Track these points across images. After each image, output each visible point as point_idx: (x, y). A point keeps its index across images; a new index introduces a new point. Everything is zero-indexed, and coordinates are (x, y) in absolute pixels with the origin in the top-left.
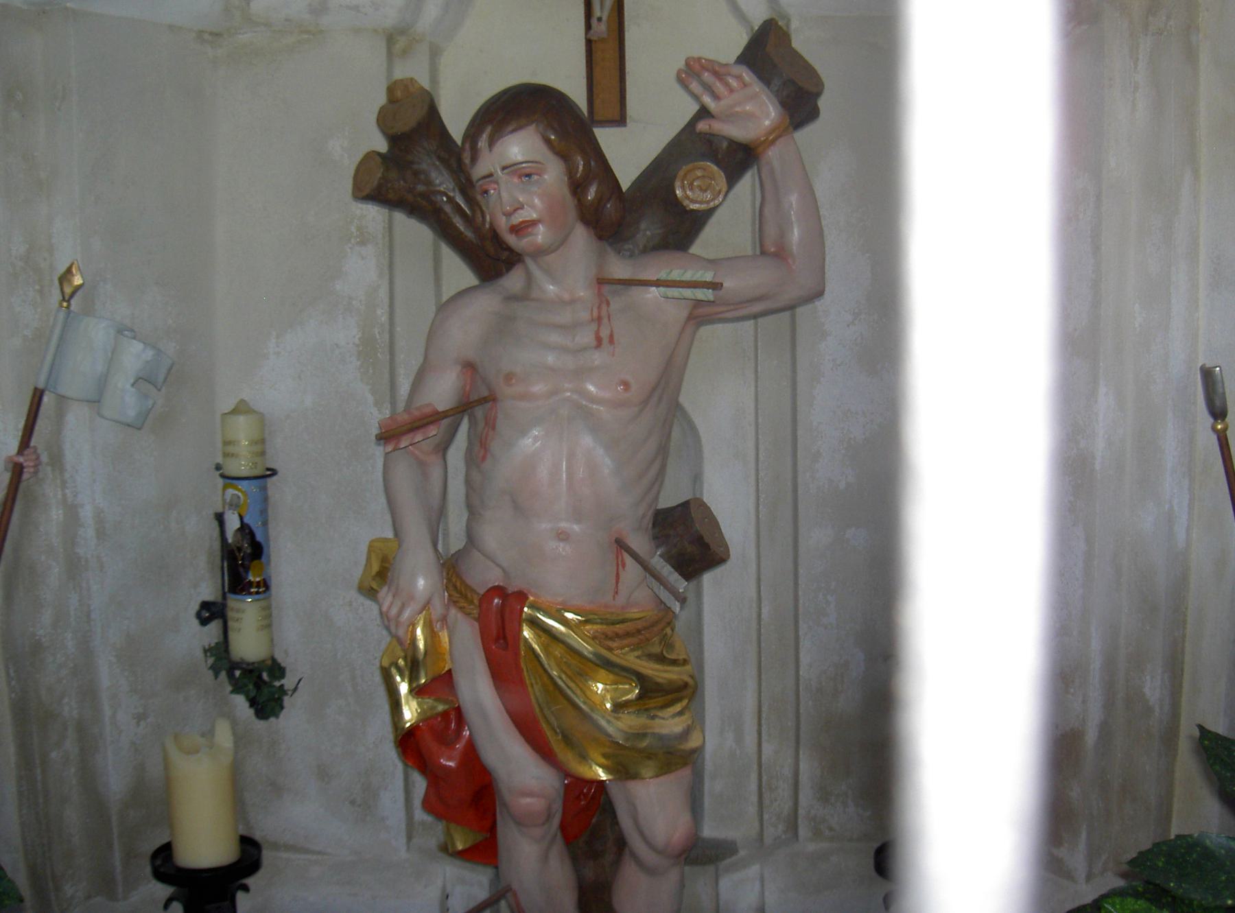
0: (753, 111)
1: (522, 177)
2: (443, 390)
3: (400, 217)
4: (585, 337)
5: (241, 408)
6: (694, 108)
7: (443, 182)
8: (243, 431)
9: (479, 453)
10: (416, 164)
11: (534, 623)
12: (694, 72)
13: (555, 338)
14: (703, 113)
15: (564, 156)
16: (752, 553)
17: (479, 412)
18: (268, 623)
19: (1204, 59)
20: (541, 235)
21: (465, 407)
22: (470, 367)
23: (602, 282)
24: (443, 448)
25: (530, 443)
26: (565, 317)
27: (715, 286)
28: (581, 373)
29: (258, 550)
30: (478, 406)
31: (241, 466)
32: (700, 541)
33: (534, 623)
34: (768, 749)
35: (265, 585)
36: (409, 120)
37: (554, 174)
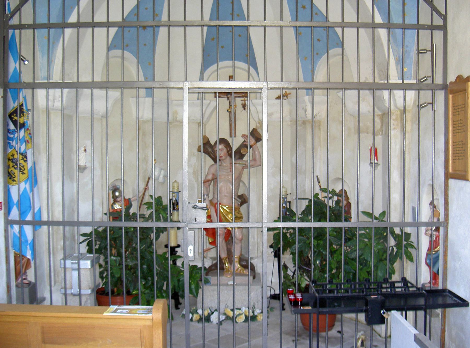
0: (251, 141)
1: (220, 150)
2: (210, 177)
3: (207, 155)
4: (229, 171)
5: (176, 181)
6: (243, 140)
7: (210, 150)
8: (176, 185)
9: (215, 184)
10: (208, 148)
11: (222, 207)
12: (244, 136)
13: (225, 171)
14: (245, 141)
15: (227, 148)
16: (256, 207)
17: (215, 180)
18: (178, 216)
19: (322, 130)
20: (223, 158)
21: (213, 179)
22: (213, 174)
23: (343, 180)
24: (209, 185)
25: (221, 184)
26: (226, 168)
27: (245, 164)
28: (228, 175)
29: (177, 204)
30: (214, 179)
31: (176, 190)
32: (245, 200)
33: (222, 207)
34: (259, 240)
35: (178, 209)
36: (206, 141)
37: (225, 150)
